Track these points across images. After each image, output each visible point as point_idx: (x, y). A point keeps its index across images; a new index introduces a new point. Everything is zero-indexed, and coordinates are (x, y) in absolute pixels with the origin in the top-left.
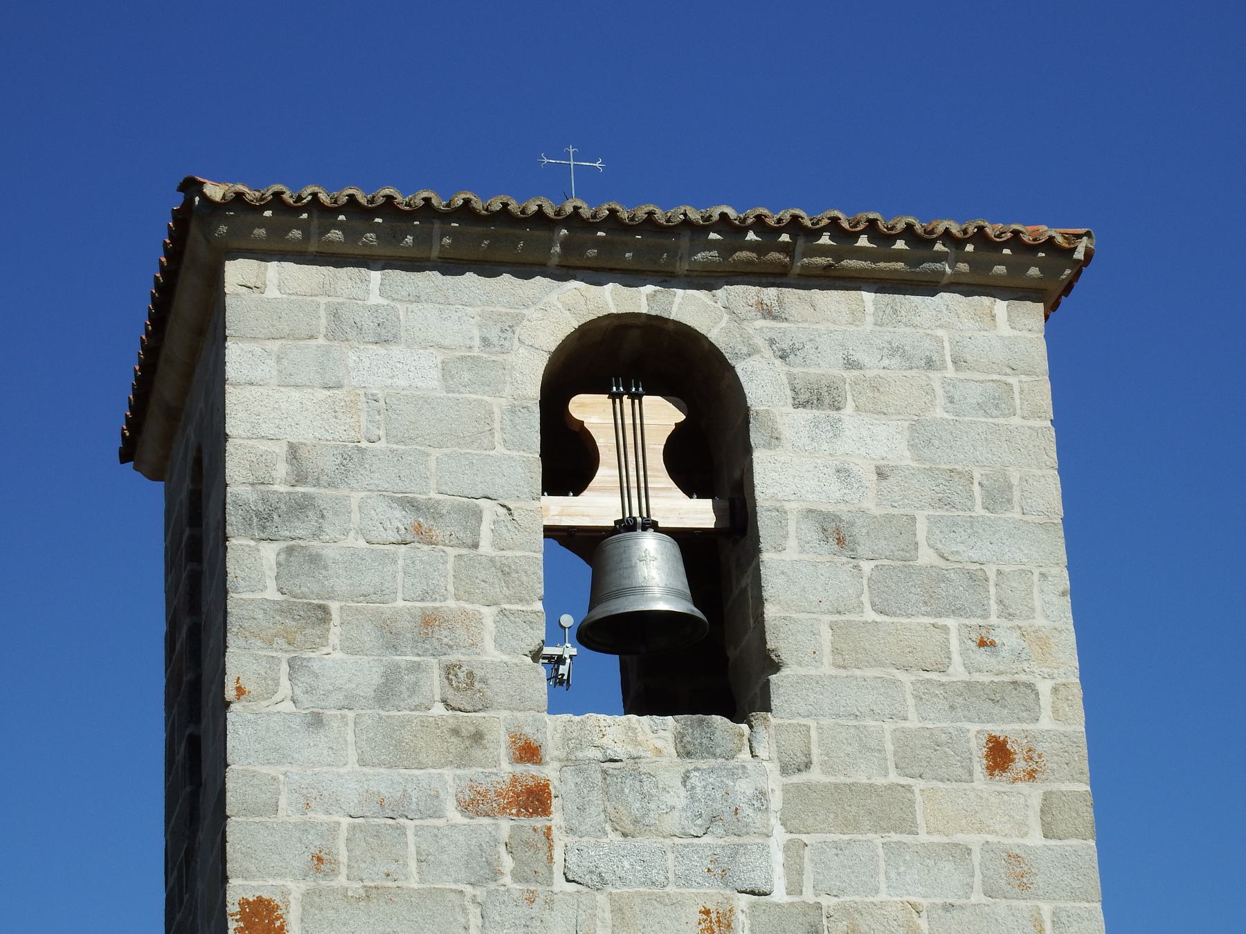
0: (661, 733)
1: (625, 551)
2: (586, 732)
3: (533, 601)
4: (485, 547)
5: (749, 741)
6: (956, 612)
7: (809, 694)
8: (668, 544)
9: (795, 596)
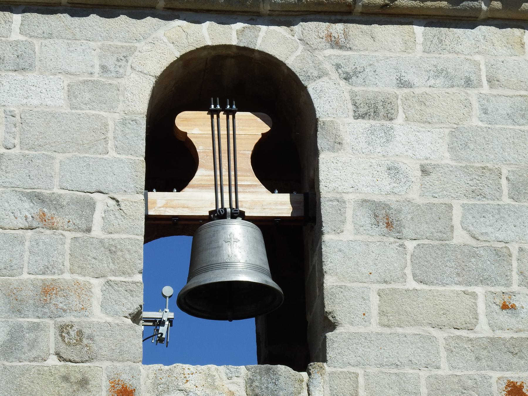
0: (235, 379)
1: (214, 235)
3: (134, 274)
4: (97, 231)
5: (308, 385)
6: (483, 281)
7: (358, 348)
8: (250, 229)
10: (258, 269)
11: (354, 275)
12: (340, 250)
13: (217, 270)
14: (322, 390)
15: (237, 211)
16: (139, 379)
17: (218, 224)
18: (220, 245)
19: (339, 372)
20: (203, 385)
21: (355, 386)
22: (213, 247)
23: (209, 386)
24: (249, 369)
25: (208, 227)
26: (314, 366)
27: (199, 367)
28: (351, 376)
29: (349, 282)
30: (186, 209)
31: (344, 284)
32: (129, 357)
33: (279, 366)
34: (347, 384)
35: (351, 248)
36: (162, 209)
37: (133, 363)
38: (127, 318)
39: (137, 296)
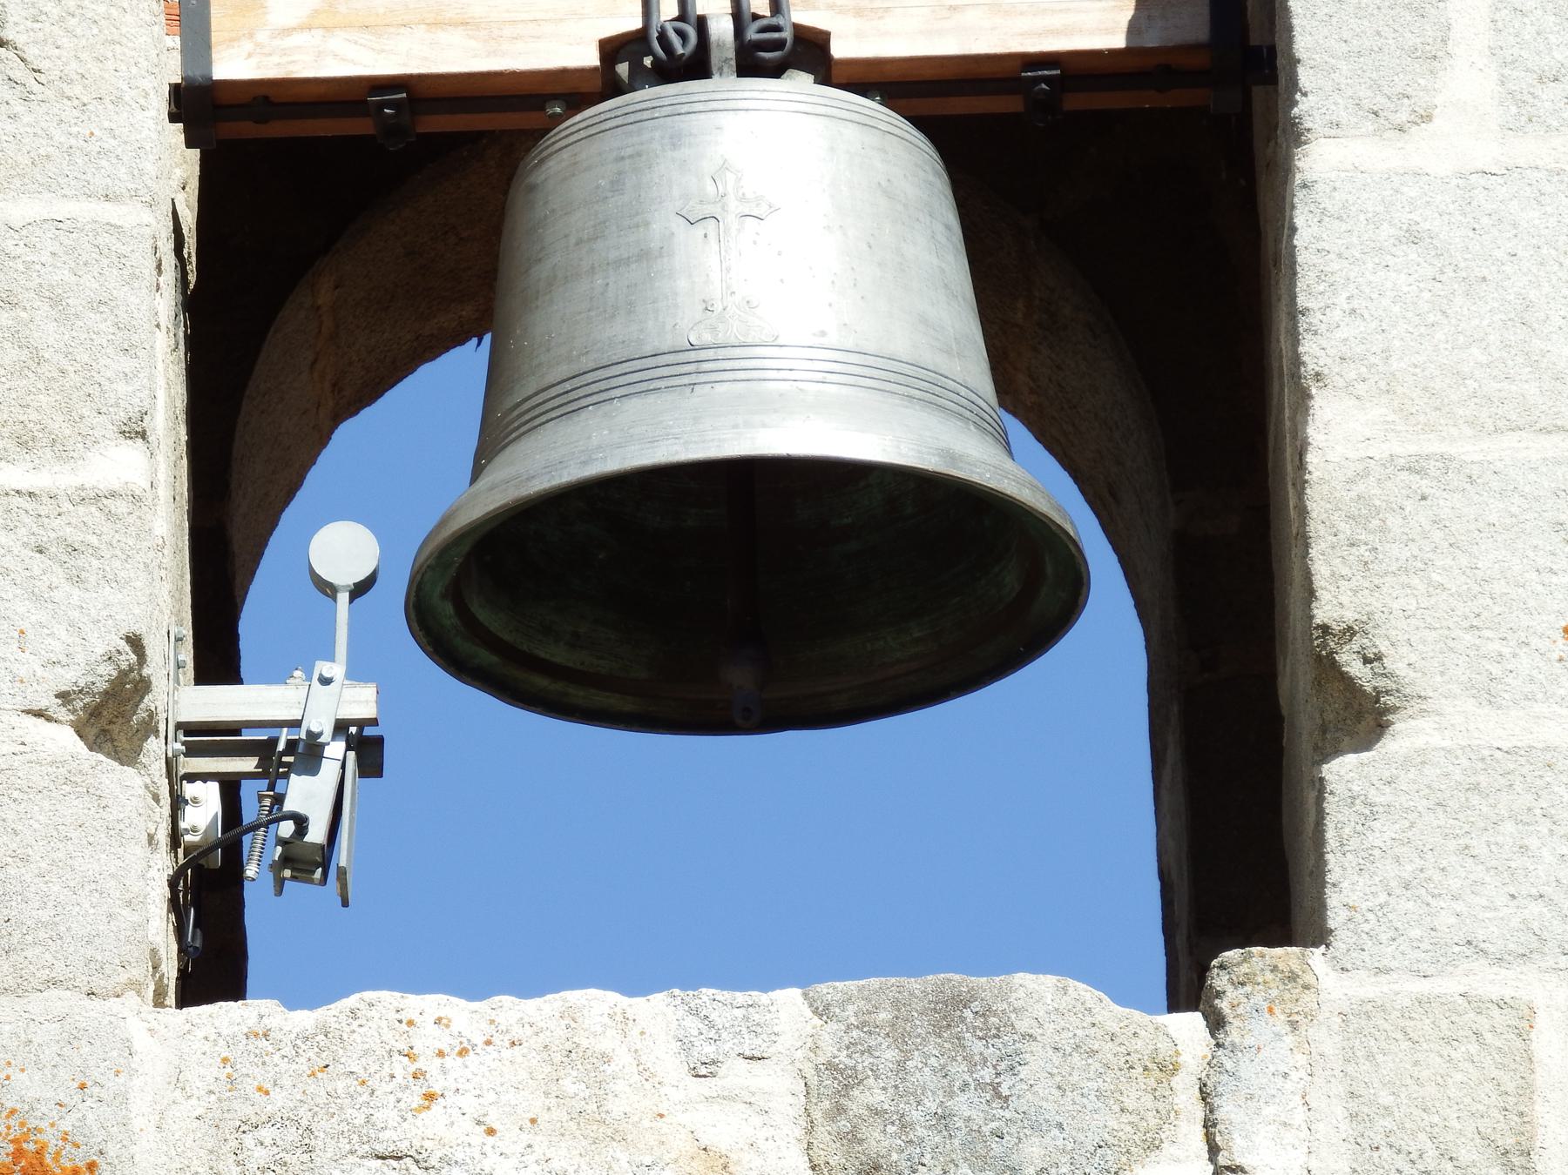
0: (736, 1074)
1: (617, 185)
2: (340, 1085)
3: (89, 441)
5: (1204, 1096)
7: (1533, 842)
8: (851, 132)
9: (1475, 351)
10: (901, 379)
11: (1505, 385)
12: (1413, 237)
13: (635, 401)
14: (1300, 1116)
15: (777, 29)
16: (123, 1098)
17: (646, 115)
18: (655, 245)
19: (1407, 1002)
20: (533, 1121)
21: (1510, 1087)
22: (613, 255)
23: (573, 1125)
24: (827, 1007)
25: (583, 134)
26: (1245, 968)
27: (509, 1009)
28: (1483, 1024)
29: (1468, 431)
30: (455, 37)
31: (1433, 446)
32: (60, 965)
33: (1023, 979)
34: (1459, 1077)
35: (1485, 220)
36: (298, 39)
37: (86, 1002)
38: (49, 719)
39: (114, 581)
